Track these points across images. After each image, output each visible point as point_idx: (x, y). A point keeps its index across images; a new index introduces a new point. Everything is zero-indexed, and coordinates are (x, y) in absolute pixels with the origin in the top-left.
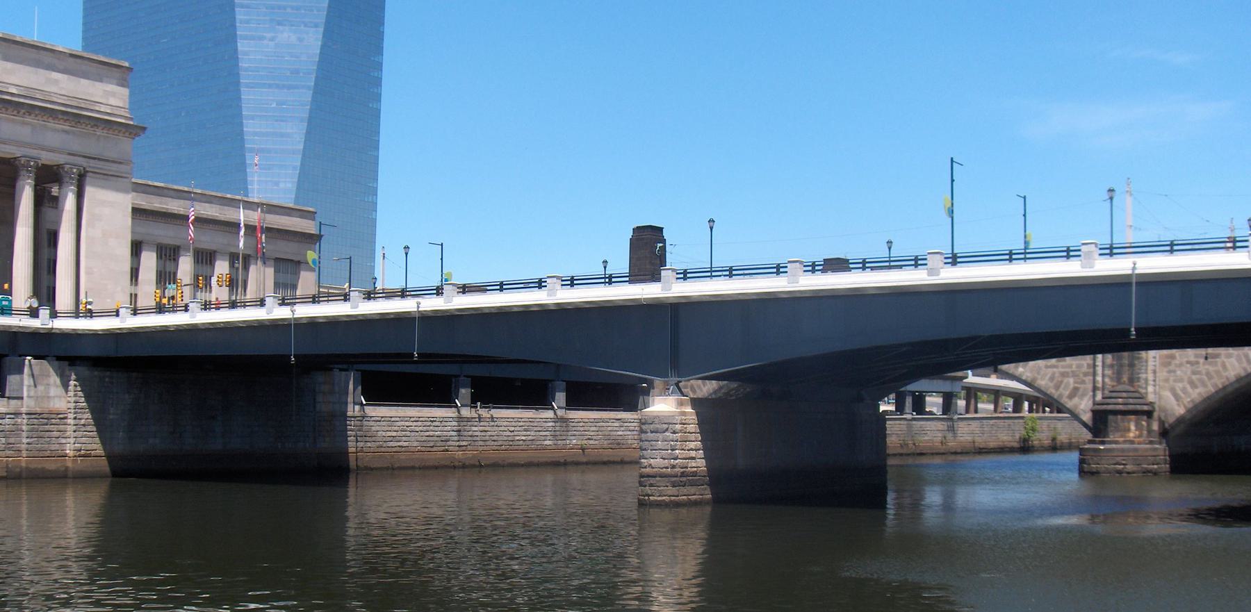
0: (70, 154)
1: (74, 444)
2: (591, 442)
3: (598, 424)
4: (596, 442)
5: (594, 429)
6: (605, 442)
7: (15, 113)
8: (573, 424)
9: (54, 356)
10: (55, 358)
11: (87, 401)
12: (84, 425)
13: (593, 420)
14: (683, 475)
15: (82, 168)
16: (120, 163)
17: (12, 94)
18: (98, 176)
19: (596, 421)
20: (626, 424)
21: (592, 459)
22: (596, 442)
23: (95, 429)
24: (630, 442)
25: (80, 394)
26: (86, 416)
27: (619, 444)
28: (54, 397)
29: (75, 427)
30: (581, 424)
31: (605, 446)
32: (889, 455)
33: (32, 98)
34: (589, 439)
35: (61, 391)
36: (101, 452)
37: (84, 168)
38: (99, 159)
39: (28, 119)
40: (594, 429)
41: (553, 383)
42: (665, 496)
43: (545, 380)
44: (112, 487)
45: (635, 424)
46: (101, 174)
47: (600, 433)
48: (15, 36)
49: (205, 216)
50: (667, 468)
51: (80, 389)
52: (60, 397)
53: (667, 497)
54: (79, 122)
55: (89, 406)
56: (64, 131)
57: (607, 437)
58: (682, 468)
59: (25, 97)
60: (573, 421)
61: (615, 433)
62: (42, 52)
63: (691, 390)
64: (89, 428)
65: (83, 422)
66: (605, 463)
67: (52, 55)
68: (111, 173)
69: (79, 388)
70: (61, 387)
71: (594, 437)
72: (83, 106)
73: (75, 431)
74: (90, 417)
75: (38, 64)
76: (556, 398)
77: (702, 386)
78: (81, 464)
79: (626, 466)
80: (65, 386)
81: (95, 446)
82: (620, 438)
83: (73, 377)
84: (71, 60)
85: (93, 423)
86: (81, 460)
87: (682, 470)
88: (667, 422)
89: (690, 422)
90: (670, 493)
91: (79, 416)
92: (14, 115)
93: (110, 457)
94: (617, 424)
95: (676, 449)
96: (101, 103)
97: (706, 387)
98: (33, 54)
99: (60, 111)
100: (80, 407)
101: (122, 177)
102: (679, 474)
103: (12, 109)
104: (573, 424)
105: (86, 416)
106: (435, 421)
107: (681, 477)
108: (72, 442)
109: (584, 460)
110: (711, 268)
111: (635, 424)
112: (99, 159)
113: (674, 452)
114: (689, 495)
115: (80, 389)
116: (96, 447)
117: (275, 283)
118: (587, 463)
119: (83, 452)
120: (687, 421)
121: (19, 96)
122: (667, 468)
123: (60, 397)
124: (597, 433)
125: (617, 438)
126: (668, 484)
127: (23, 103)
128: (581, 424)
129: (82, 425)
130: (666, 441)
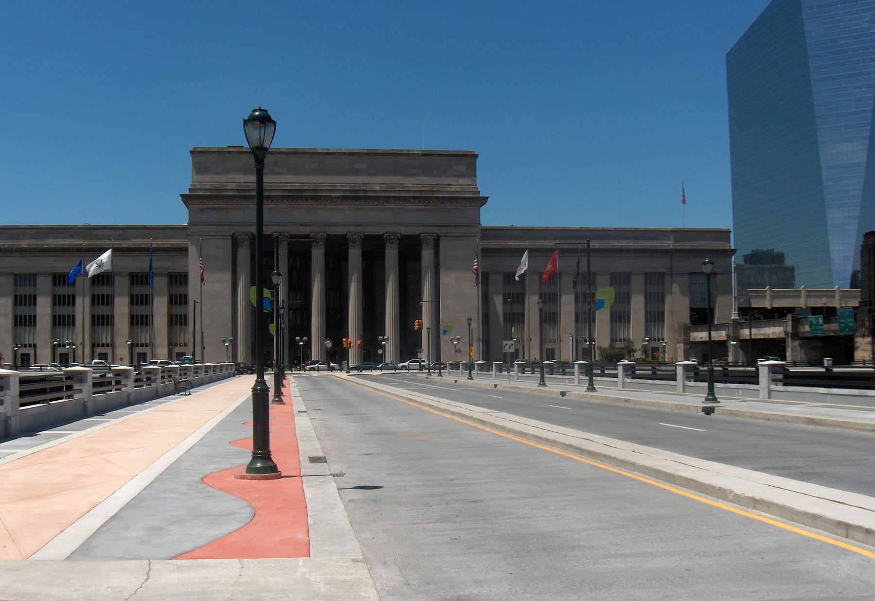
0: (424, 226)
7: (376, 203)
15: (436, 235)
16: (469, 226)
18: (112, 322)
37: (438, 235)
38: (450, 226)
39: (388, 206)
46: (452, 236)
49: (618, 247)
56: (419, 210)
68: (460, 235)
72: (436, 189)
96: (452, 185)
99: (411, 197)
101: (472, 236)
110: (429, 301)
112: (450, 226)
117: (646, 312)
127: (67, 321)
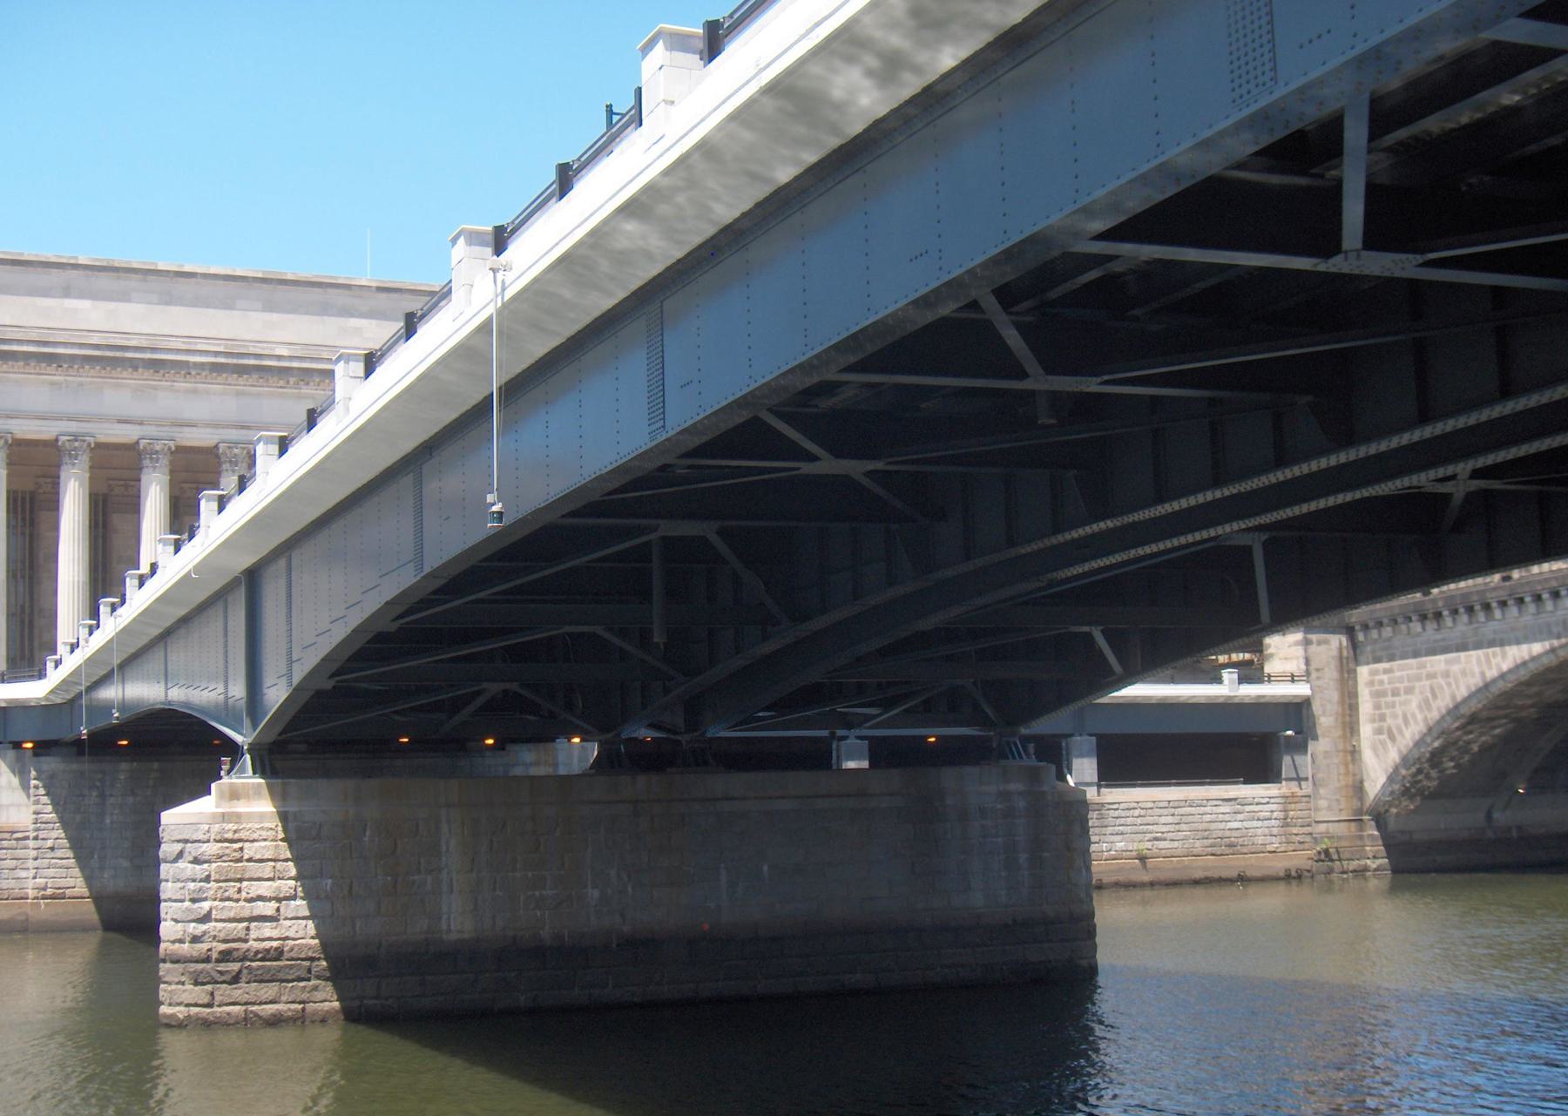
1: (35, 878)
2: (1162, 844)
3: (1177, 811)
4: (1176, 844)
5: (1170, 819)
6: (1198, 843)
8: (1116, 813)
9: (10, 743)
10: (11, 745)
11: (56, 811)
12: (52, 849)
13: (1166, 804)
14: (226, 956)
17: (279, 357)
19: (1171, 804)
20: (1248, 808)
21: (1162, 876)
22: (1176, 844)
23: (70, 854)
24: (1260, 840)
25: (45, 799)
26: (55, 834)
27: (1231, 845)
28: (8, 806)
29: (35, 852)
30: (1137, 813)
31: (1195, 851)
32: (1100, 887)
33: (312, 359)
34: (1156, 839)
35: (20, 796)
36: (85, 891)
40: (1170, 819)
41: (1069, 739)
42: (179, 1004)
43: (1054, 736)
44: (104, 950)
45: (1274, 807)
47: (1184, 827)
48: (22, 254)
50: (181, 941)
51: (43, 792)
52: (19, 806)
53: (182, 1008)
54: (189, 374)
55: (59, 818)
57: (1205, 834)
58: (225, 941)
59: (188, 352)
60: (1115, 806)
61: (1222, 826)
62: (330, 290)
63: (1390, 738)
64: (59, 853)
65: (49, 843)
66: (1196, 882)
67: (348, 292)
69: (42, 791)
70: (21, 791)
71: (1170, 835)
73: (36, 859)
74: (63, 835)
75: (324, 310)
76: (1075, 766)
77: (1404, 728)
78: (45, 911)
79: (1253, 889)
80: (25, 786)
81: (71, 882)
82: (1235, 834)
83: (33, 773)
84: (383, 296)
85: (68, 845)
86: (46, 905)
87: (223, 947)
88: (181, 837)
89: (255, 836)
90: (187, 998)
91: (42, 834)
92: (281, 387)
93: (98, 899)
94: (1226, 808)
95: (205, 899)
97: (1410, 730)
98: (316, 295)
100: (44, 820)
102: (215, 955)
103: (275, 379)
104: (1116, 813)
105: (55, 834)
106: (1117, 809)
107: (218, 961)
108: (31, 875)
109: (1146, 878)
111: (1274, 807)
113: (197, 905)
114: (253, 1004)
115: (43, 792)
116: (76, 883)
118: (1152, 884)
119: (49, 892)
120: (242, 835)
121: (291, 358)
122: (181, 941)
123: (19, 806)
124: (1177, 827)
125: (1228, 833)
126: (183, 978)
128: (1137, 813)
129: (49, 848)
130: (178, 880)
